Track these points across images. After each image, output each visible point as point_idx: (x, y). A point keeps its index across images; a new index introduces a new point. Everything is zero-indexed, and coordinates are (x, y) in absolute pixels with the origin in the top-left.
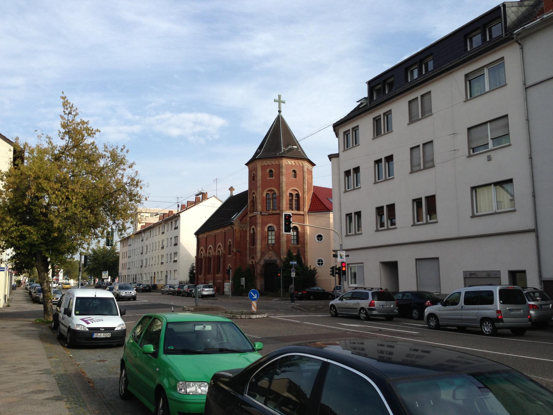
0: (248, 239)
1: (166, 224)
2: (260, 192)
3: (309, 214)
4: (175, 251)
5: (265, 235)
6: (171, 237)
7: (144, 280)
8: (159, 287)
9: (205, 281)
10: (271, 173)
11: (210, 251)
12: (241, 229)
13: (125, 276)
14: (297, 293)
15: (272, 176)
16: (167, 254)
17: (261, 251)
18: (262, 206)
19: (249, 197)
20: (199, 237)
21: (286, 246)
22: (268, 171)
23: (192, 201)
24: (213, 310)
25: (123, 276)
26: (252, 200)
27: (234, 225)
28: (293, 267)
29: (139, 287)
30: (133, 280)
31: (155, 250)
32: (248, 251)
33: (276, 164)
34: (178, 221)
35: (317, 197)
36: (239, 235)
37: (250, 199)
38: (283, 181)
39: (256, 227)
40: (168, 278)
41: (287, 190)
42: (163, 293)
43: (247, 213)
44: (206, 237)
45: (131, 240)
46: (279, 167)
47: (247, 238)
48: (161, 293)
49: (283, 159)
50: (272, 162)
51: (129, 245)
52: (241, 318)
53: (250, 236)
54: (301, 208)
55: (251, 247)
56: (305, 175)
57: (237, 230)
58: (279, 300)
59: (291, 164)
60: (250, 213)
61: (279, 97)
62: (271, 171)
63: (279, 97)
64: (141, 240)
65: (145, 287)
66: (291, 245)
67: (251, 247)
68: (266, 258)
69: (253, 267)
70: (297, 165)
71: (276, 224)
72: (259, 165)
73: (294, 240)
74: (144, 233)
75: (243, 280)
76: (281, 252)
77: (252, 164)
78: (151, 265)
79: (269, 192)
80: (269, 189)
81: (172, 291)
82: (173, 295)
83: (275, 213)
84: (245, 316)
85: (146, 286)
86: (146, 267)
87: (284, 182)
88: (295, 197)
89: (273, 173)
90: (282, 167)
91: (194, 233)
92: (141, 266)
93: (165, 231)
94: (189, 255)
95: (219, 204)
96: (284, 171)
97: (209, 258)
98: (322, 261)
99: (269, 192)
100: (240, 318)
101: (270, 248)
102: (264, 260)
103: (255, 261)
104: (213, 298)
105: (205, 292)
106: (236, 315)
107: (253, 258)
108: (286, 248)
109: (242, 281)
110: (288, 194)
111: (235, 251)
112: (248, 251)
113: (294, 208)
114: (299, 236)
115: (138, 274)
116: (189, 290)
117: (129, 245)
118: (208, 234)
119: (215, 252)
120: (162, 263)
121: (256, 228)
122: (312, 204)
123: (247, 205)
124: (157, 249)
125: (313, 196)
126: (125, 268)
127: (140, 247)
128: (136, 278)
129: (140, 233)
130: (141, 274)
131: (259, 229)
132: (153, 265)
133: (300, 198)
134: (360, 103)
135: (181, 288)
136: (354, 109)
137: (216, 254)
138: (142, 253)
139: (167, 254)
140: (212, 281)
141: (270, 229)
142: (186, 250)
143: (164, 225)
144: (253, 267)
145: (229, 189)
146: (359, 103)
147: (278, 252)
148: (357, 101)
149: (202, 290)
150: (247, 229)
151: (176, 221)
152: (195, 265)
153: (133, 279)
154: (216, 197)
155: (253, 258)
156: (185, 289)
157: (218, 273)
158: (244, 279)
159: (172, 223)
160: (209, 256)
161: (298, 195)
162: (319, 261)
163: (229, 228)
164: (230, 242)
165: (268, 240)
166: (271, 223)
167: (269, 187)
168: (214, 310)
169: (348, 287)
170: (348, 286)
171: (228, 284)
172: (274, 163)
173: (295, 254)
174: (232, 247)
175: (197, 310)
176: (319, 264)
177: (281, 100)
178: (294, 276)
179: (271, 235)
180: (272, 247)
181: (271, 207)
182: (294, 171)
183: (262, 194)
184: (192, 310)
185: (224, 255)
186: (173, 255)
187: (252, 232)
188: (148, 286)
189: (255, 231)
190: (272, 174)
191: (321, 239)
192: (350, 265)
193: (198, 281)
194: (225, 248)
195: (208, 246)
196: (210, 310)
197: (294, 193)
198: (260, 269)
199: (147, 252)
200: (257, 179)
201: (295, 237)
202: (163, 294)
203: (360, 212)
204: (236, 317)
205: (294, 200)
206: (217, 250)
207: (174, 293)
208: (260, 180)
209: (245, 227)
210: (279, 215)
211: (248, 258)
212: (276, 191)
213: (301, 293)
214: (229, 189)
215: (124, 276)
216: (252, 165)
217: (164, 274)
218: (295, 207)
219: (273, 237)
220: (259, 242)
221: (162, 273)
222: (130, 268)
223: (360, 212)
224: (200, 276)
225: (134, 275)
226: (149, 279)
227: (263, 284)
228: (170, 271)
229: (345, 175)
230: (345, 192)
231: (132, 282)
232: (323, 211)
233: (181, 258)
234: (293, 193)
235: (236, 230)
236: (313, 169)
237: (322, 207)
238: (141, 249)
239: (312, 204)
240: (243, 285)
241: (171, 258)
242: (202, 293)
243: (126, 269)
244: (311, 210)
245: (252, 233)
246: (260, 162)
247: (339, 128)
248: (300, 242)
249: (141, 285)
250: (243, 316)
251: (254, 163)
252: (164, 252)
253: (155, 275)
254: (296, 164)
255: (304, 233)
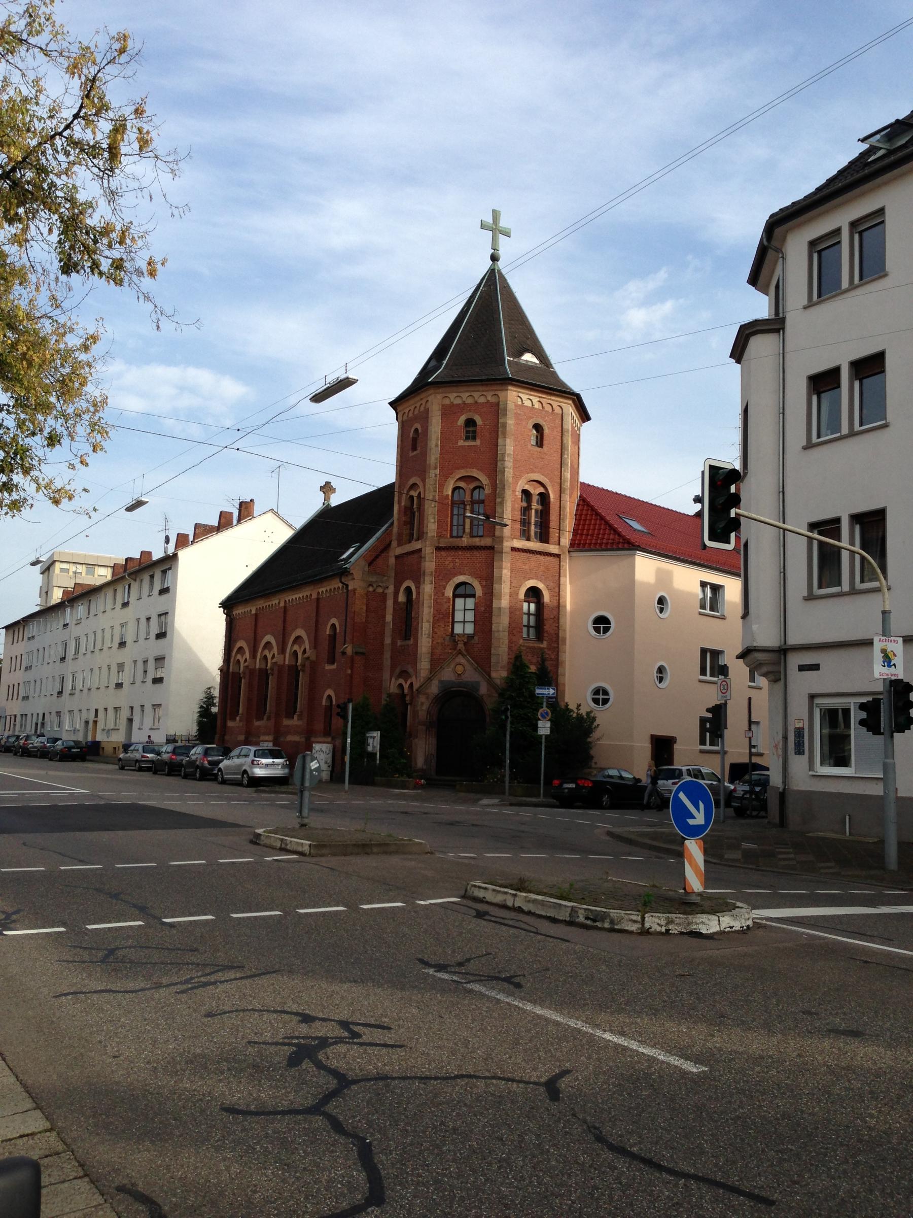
0: (389, 618)
1: (135, 580)
2: (436, 481)
3: (573, 554)
4: (158, 653)
5: (446, 606)
6: (148, 614)
7: (67, 728)
8: (108, 750)
9: (246, 738)
10: (471, 429)
11: (266, 652)
12: (371, 589)
13: (15, 716)
14: (561, 785)
15: (474, 438)
16: (135, 662)
17: (432, 654)
18: (440, 523)
19: (396, 499)
20: (234, 613)
21: (506, 642)
22: (462, 420)
23: (207, 525)
24: (385, 853)
25: (8, 718)
26: (406, 507)
27: (350, 577)
28: (545, 704)
29: (54, 747)
30: (36, 729)
31: (101, 650)
32: (387, 655)
33: (488, 401)
34: (170, 571)
35: (593, 509)
36: (364, 608)
37: (399, 502)
38: (508, 452)
39: (418, 583)
40: (136, 724)
41: (516, 478)
42: (123, 765)
43: (389, 545)
44: (256, 615)
45: (35, 625)
46: (497, 411)
47: (384, 617)
48: (117, 767)
49: (510, 388)
50: (476, 395)
51: (29, 638)
52: (645, 932)
53: (394, 609)
54: (554, 534)
55: (398, 644)
56: (568, 440)
57: (360, 591)
58: (497, 805)
59: (530, 405)
60: (399, 545)
61: (496, 215)
62: (470, 423)
63: (496, 215)
64: (61, 624)
65: (70, 748)
66: (521, 641)
67: (399, 643)
68: (448, 674)
69: (402, 701)
70: (546, 409)
71: (479, 578)
72: (435, 402)
73: (528, 626)
74: (72, 607)
75: (374, 738)
76: (493, 660)
77: (412, 402)
78: (85, 691)
79: (462, 484)
80: (462, 473)
81: (152, 762)
82: (155, 773)
83: (478, 544)
84: (663, 922)
85: (72, 744)
86: (74, 694)
87: (509, 455)
88: (538, 503)
89: (478, 429)
90: (506, 410)
91: (220, 601)
92: (60, 693)
93: (132, 600)
94: (199, 668)
95: (283, 535)
96: (510, 422)
97: (264, 674)
98: (605, 692)
99: (462, 484)
100: (634, 927)
101: (461, 646)
102: (441, 682)
103: (411, 684)
104: (284, 788)
105: (261, 768)
106: (614, 913)
107: (404, 674)
108: (506, 649)
109: (370, 741)
110: (519, 494)
111: (349, 650)
112: (387, 655)
113: (532, 533)
114: (545, 618)
115: (50, 713)
116: (208, 761)
117: (29, 638)
118: (261, 603)
119: (283, 656)
120: (119, 686)
121: (418, 588)
122: (580, 527)
123: (390, 521)
124: (105, 648)
125: (580, 507)
126: (15, 697)
127: (60, 643)
128: (43, 724)
129: (60, 606)
130: (58, 713)
131: (428, 588)
132: (93, 690)
133: (552, 506)
134: (868, 146)
135: (182, 754)
136: (849, 163)
137: (287, 663)
138: (63, 659)
139: (135, 662)
140: (271, 738)
141: (462, 590)
142: (189, 650)
143: (129, 585)
144: (402, 701)
145: (321, 487)
146: (864, 146)
147: (483, 663)
148: (861, 137)
149: (252, 763)
150: (386, 591)
151: (164, 572)
152: (216, 693)
153: (37, 724)
154: (276, 514)
155: (404, 674)
156: (194, 758)
157: (290, 716)
158: (377, 734)
159: (152, 577)
160: (263, 666)
161: (544, 498)
162: (597, 692)
163: (336, 584)
164: (333, 626)
165: (453, 622)
166: (465, 574)
167: (463, 468)
168: (390, 853)
169: (813, 776)
170: (811, 773)
171: (324, 749)
172: (482, 400)
173: (533, 669)
174: (340, 639)
175: (324, 851)
176: (596, 701)
177: (501, 225)
178: (548, 732)
179: (463, 608)
180: (465, 644)
181: (468, 529)
182: (538, 427)
183: (442, 486)
184: (300, 849)
185: (314, 666)
186: (151, 665)
187: (402, 598)
188: (77, 743)
189: (414, 596)
190: (474, 432)
191: (606, 630)
192: (818, 701)
193: (224, 735)
194: (315, 644)
195: (236, 641)
196: (375, 850)
197: (536, 491)
198: (425, 707)
199: (76, 656)
200: (426, 444)
201: (532, 618)
202: (122, 768)
203: (880, 515)
204: (612, 922)
205: (533, 511)
206: (288, 650)
207: (157, 768)
208: (437, 446)
209: (380, 584)
210: (491, 551)
211: (386, 675)
212: (484, 480)
213: (573, 786)
214: (321, 487)
215: (13, 718)
216: (409, 407)
217: (125, 714)
218: (536, 533)
219: (470, 616)
220: (425, 627)
221: (117, 711)
222: (28, 697)
223: (880, 515)
224: (230, 724)
225: (38, 714)
226: (79, 725)
227: (434, 752)
228: (142, 706)
229: (808, 387)
230: (809, 446)
231: (33, 732)
232: (615, 547)
233: (175, 671)
234: (532, 491)
235: (355, 590)
236: (582, 429)
237: (612, 536)
238: (60, 648)
239: (580, 527)
240: (376, 754)
241: (145, 672)
242: (253, 773)
243: (17, 699)
244: (580, 544)
245: (404, 603)
246: (439, 393)
247: (787, 232)
248: (545, 635)
249: (59, 743)
250: (654, 922)
251: (417, 398)
252: (125, 656)
253: (96, 716)
254: (543, 408)
255: (558, 607)
